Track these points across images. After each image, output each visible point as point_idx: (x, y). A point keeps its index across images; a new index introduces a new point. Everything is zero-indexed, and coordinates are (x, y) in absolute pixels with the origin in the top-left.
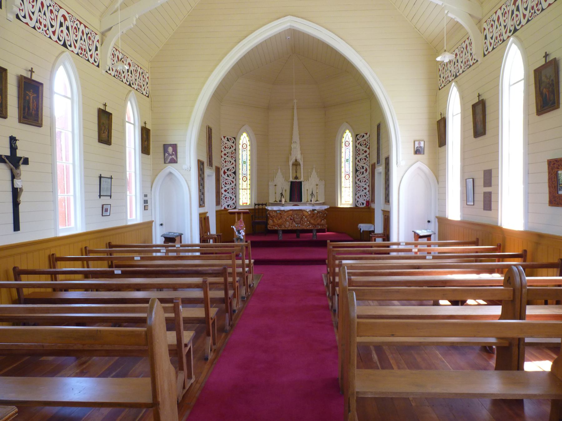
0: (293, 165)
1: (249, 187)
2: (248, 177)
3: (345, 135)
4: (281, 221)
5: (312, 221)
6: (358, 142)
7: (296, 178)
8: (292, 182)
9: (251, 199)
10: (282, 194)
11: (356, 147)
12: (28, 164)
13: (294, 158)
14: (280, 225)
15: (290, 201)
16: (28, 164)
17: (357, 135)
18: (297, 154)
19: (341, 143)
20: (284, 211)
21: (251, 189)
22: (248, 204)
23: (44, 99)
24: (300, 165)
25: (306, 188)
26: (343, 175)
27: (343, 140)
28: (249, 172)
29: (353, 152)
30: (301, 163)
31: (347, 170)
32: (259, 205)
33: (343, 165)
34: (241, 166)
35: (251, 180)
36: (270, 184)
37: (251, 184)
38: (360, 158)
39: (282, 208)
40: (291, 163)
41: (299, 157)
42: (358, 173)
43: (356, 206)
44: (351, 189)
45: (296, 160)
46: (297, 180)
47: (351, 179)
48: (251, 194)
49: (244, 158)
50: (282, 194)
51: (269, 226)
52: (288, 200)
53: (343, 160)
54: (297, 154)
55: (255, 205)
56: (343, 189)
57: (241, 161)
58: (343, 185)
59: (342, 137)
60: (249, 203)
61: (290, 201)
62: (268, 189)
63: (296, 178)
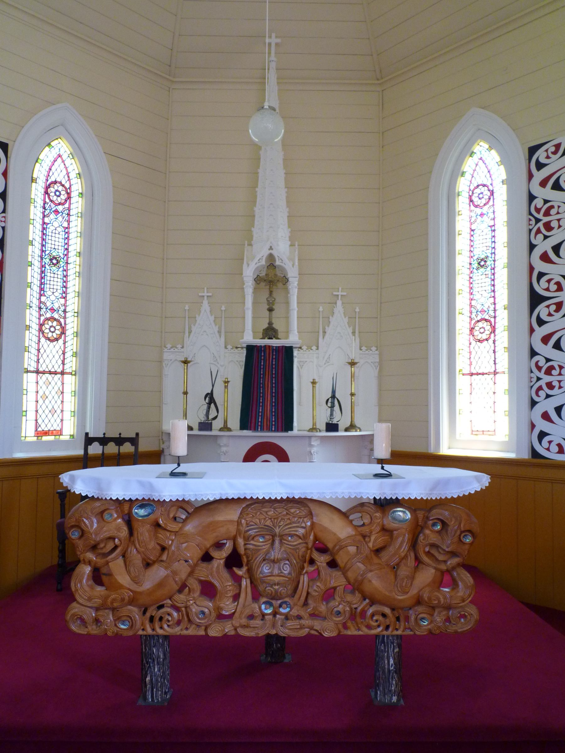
0: (258, 280)
1: (71, 364)
2: (72, 324)
3: (469, 165)
4: (158, 573)
5: (376, 582)
6: (539, 176)
7: (270, 332)
8: (251, 349)
9: (80, 414)
10: (210, 398)
11: (532, 198)
12: (541, 431)
13: (265, 252)
14: (151, 606)
15: (244, 425)
16: (541, 431)
17: (533, 150)
18: (273, 237)
19: (452, 196)
20: (181, 504)
21: (82, 373)
22: (65, 437)
23: (5, 292)
24: (285, 280)
25: (308, 374)
26: (462, 324)
27: (463, 185)
28: (73, 303)
29: (510, 223)
30: (293, 273)
31: (483, 300)
32: (104, 441)
33: (461, 282)
34: (33, 275)
35: (84, 334)
36: (167, 356)
37: (82, 355)
38: (553, 241)
39: (170, 490)
40: (249, 273)
41: (283, 250)
42: (542, 310)
43: (535, 454)
44: (503, 381)
45: (271, 257)
46: (274, 343)
47: (503, 338)
48: (81, 394)
49: (55, 244)
50: (210, 398)
51: (74, 609)
52: (234, 421)
53: (462, 262)
54: (273, 237)
55: (89, 441)
56: (462, 382)
57: (34, 251)
58: (461, 363)
59: (457, 172)
60: (69, 429)
61: (244, 425)
62: (160, 376)
63: (270, 332)
